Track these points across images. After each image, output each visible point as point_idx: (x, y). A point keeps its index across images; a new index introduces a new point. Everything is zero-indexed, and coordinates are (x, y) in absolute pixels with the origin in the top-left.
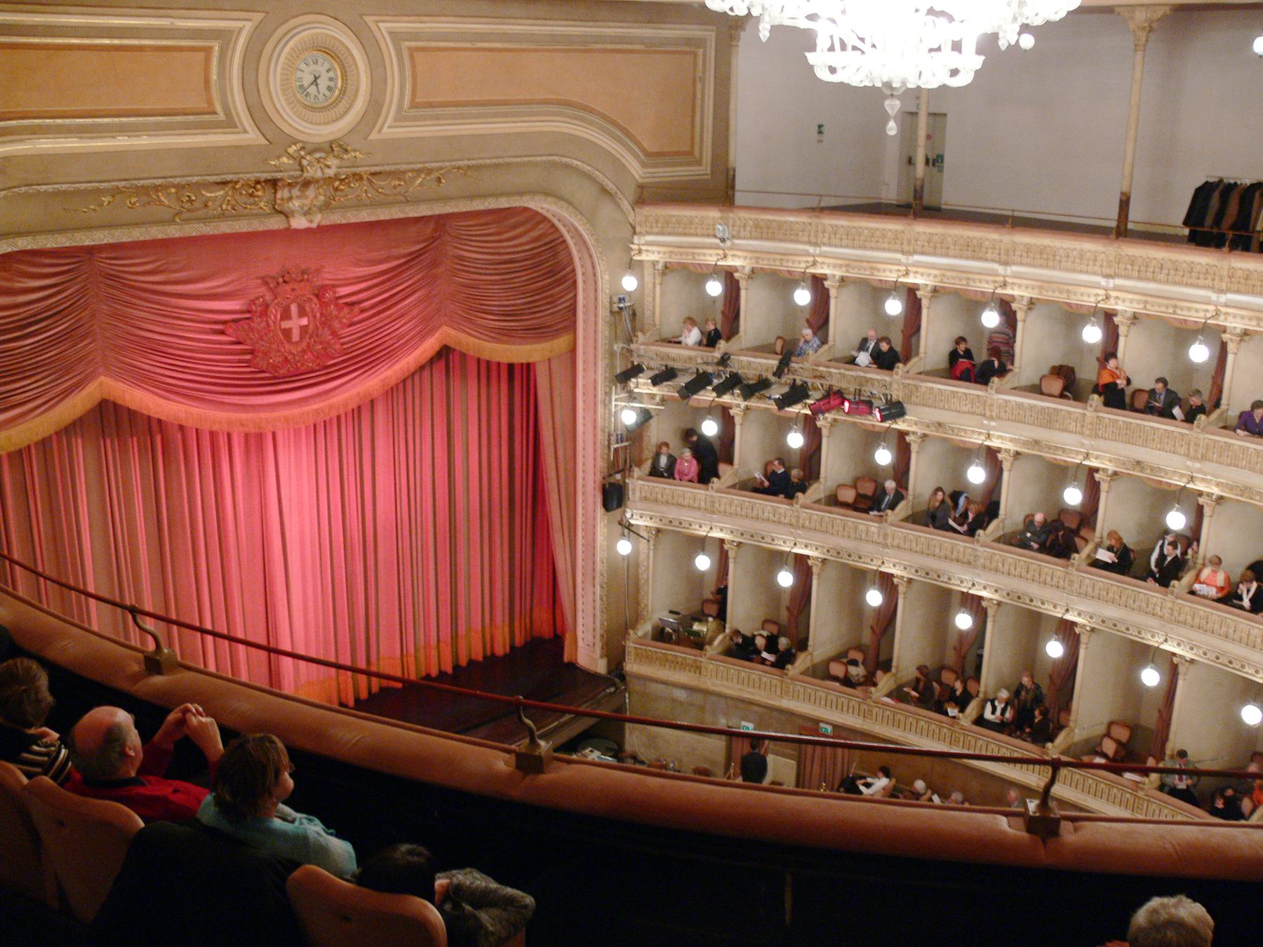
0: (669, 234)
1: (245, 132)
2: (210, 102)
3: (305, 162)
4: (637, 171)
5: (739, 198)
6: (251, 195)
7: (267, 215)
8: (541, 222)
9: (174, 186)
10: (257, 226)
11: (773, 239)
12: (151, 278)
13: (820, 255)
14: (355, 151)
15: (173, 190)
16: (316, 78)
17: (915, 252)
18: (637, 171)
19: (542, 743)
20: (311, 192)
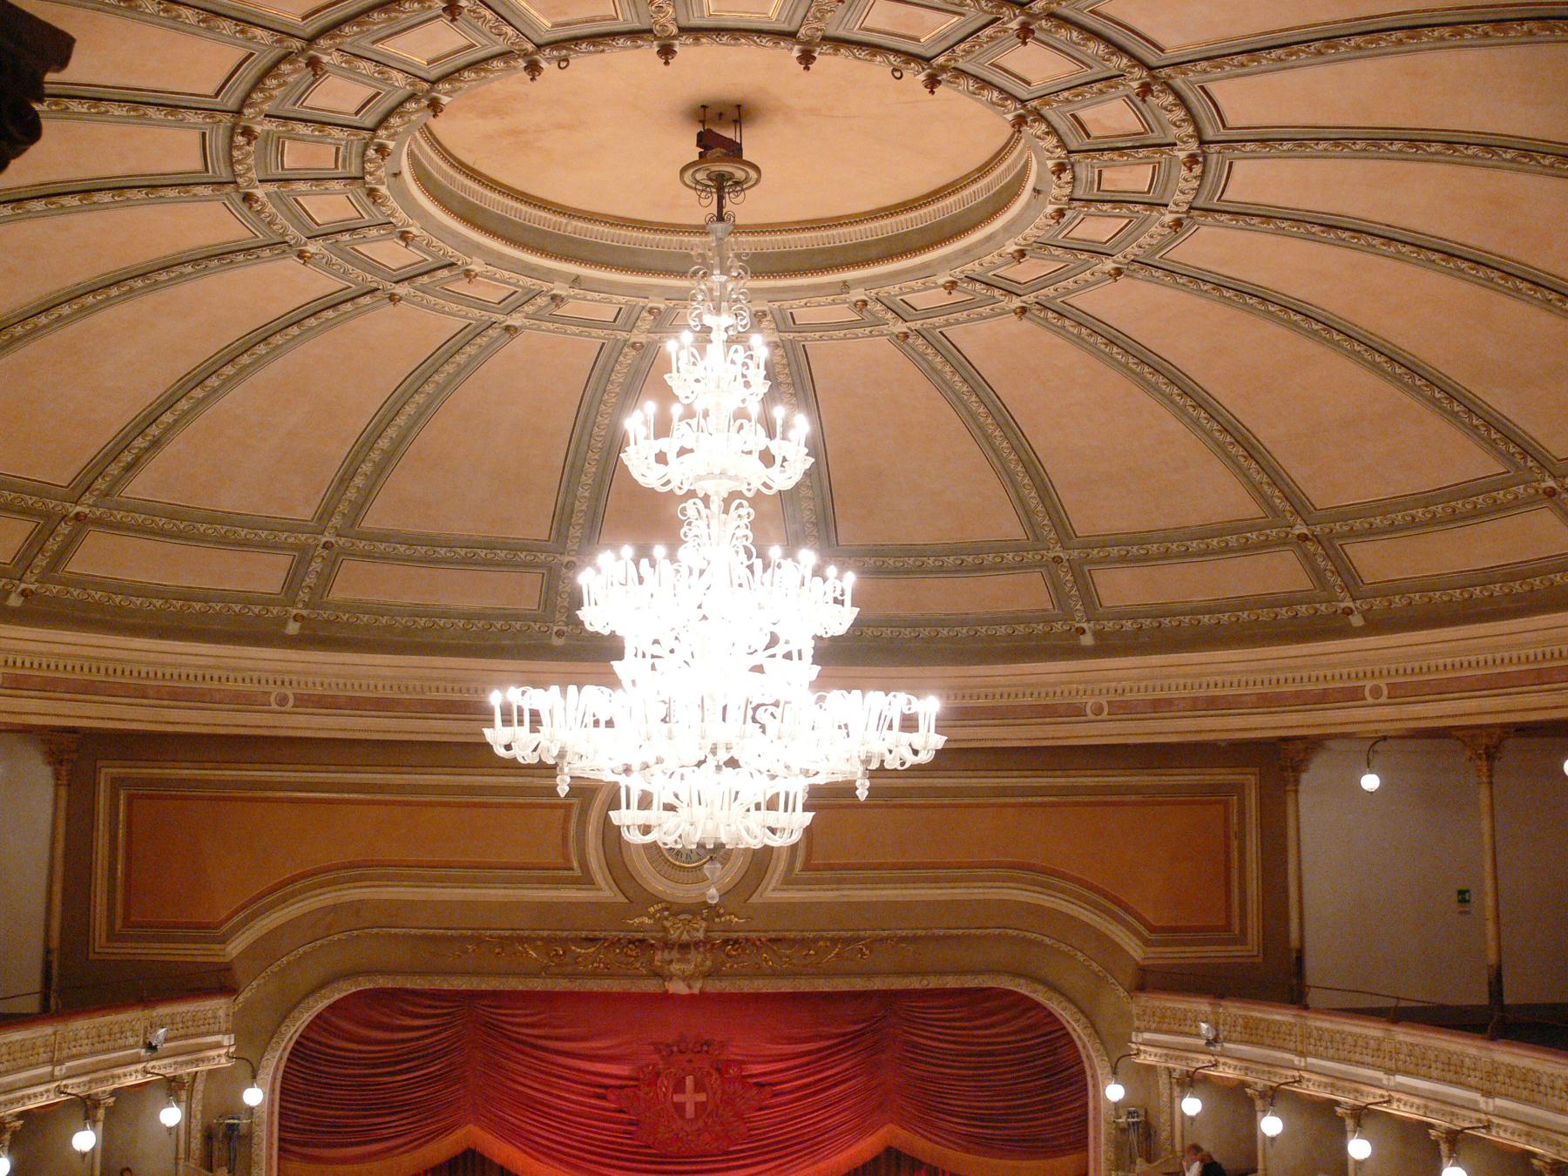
2: (568, 860)
4: (1136, 950)
5: (1313, 997)
7: (642, 976)
8: (1029, 1010)
9: (542, 939)
12: (536, 1032)
17: (1396, 1071)
18: (1136, 950)
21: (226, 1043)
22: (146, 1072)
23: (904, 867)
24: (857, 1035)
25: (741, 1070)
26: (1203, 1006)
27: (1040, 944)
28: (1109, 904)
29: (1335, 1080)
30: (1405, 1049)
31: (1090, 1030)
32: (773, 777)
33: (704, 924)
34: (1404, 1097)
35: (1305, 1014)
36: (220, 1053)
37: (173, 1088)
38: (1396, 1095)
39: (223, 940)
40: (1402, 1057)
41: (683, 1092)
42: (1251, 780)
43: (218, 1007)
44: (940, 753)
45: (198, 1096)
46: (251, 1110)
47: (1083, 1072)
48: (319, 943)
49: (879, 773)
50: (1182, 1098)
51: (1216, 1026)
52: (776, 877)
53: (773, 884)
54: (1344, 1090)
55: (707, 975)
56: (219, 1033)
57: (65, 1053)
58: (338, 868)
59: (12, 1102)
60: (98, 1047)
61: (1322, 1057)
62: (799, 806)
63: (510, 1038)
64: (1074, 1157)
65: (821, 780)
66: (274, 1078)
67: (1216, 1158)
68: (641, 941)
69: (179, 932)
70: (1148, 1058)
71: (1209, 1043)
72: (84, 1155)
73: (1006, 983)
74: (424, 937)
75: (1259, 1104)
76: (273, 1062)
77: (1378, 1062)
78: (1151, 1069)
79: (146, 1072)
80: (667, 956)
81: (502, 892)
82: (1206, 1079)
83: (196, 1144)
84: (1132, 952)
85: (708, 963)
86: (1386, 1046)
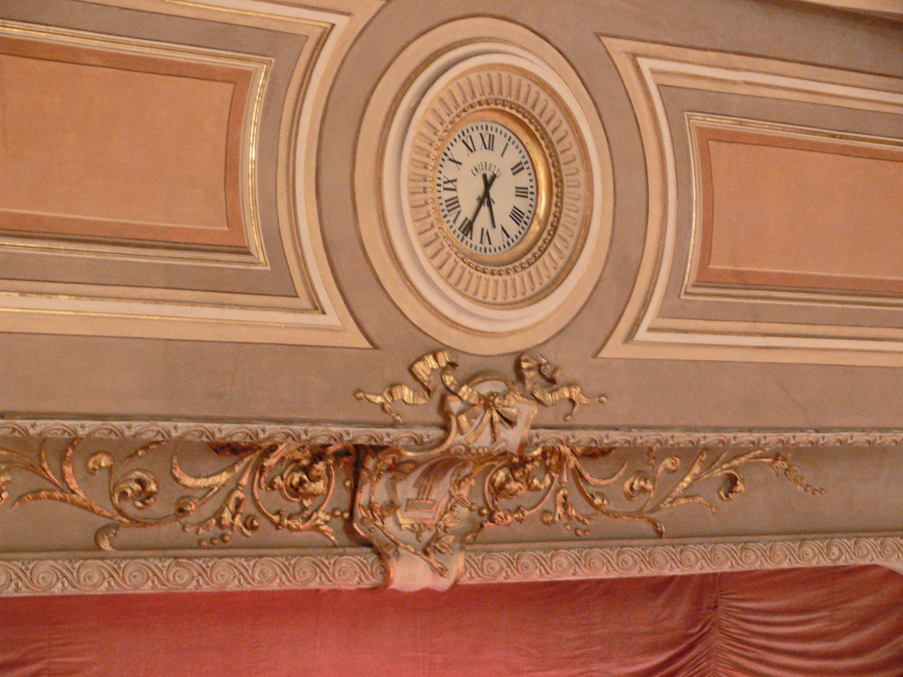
1: (317, 308)
2: (234, 220)
3: (454, 405)
6: (295, 490)
10: (307, 576)
14: (570, 385)
15: (104, 461)
16: (488, 184)
20: (440, 491)
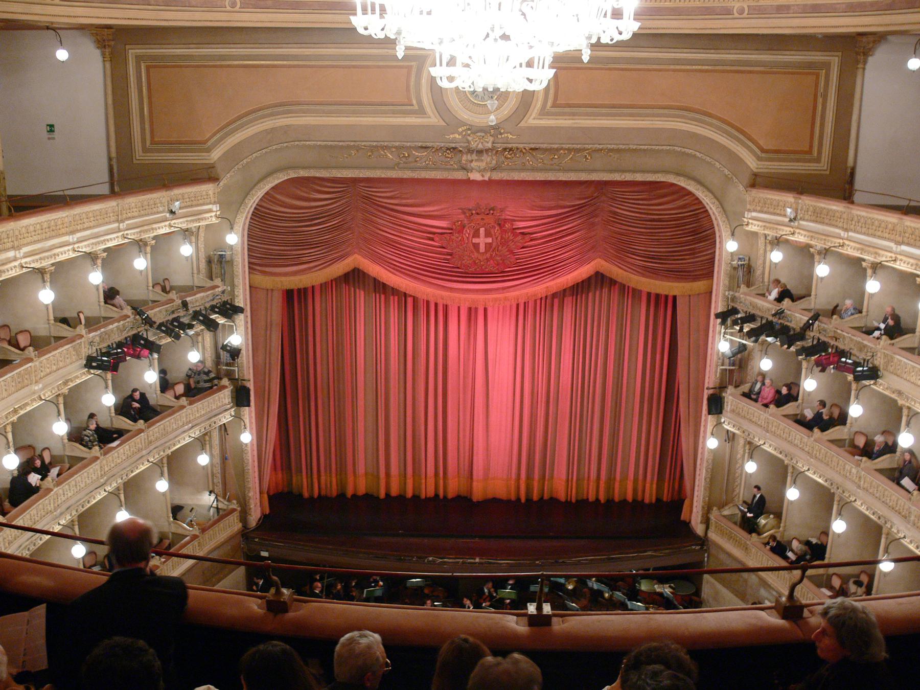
0: (766, 213)
2: (410, 99)
4: (752, 163)
5: (857, 197)
9: (396, 147)
11: (822, 223)
13: (847, 239)
17: (902, 243)
18: (752, 163)
19: (285, 591)
21: (214, 209)
22: (171, 226)
23: (614, 106)
24: (581, 207)
25: (512, 225)
26: (789, 198)
27: (694, 156)
28: (737, 134)
29: (864, 247)
30: (909, 231)
31: (720, 209)
32: (531, 47)
33: (491, 139)
34: (904, 258)
35: (851, 206)
36: (212, 215)
37: (187, 234)
38: (899, 257)
39: (208, 150)
40: (907, 235)
41: (479, 237)
42: (835, 60)
43: (208, 189)
44: (635, 35)
45: (201, 239)
46: (231, 247)
47: (714, 233)
48: (264, 151)
49: (597, 46)
50: (772, 251)
51: (796, 211)
52: (536, 111)
53: (534, 115)
54: (869, 253)
55: (493, 169)
56: (210, 203)
57: (124, 216)
58: (276, 106)
59: (98, 243)
60: (142, 212)
61: (858, 232)
62: (546, 65)
63: (378, 205)
64: (705, 282)
65: (561, 49)
66: (243, 229)
67: (788, 287)
68: (454, 148)
69: (183, 147)
70: (754, 227)
71: (791, 220)
72: (141, 272)
73: (671, 179)
74: (326, 147)
75: (817, 257)
76: (243, 219)
77: (892, 237)
78: (755, 234)
79: (171, 226)
80: (469, 157)
81: (371, 119)
82: (787, 241)
83: (203, 265)
84: (749, 164)
85: (494, 162)
86: (899, 228)
